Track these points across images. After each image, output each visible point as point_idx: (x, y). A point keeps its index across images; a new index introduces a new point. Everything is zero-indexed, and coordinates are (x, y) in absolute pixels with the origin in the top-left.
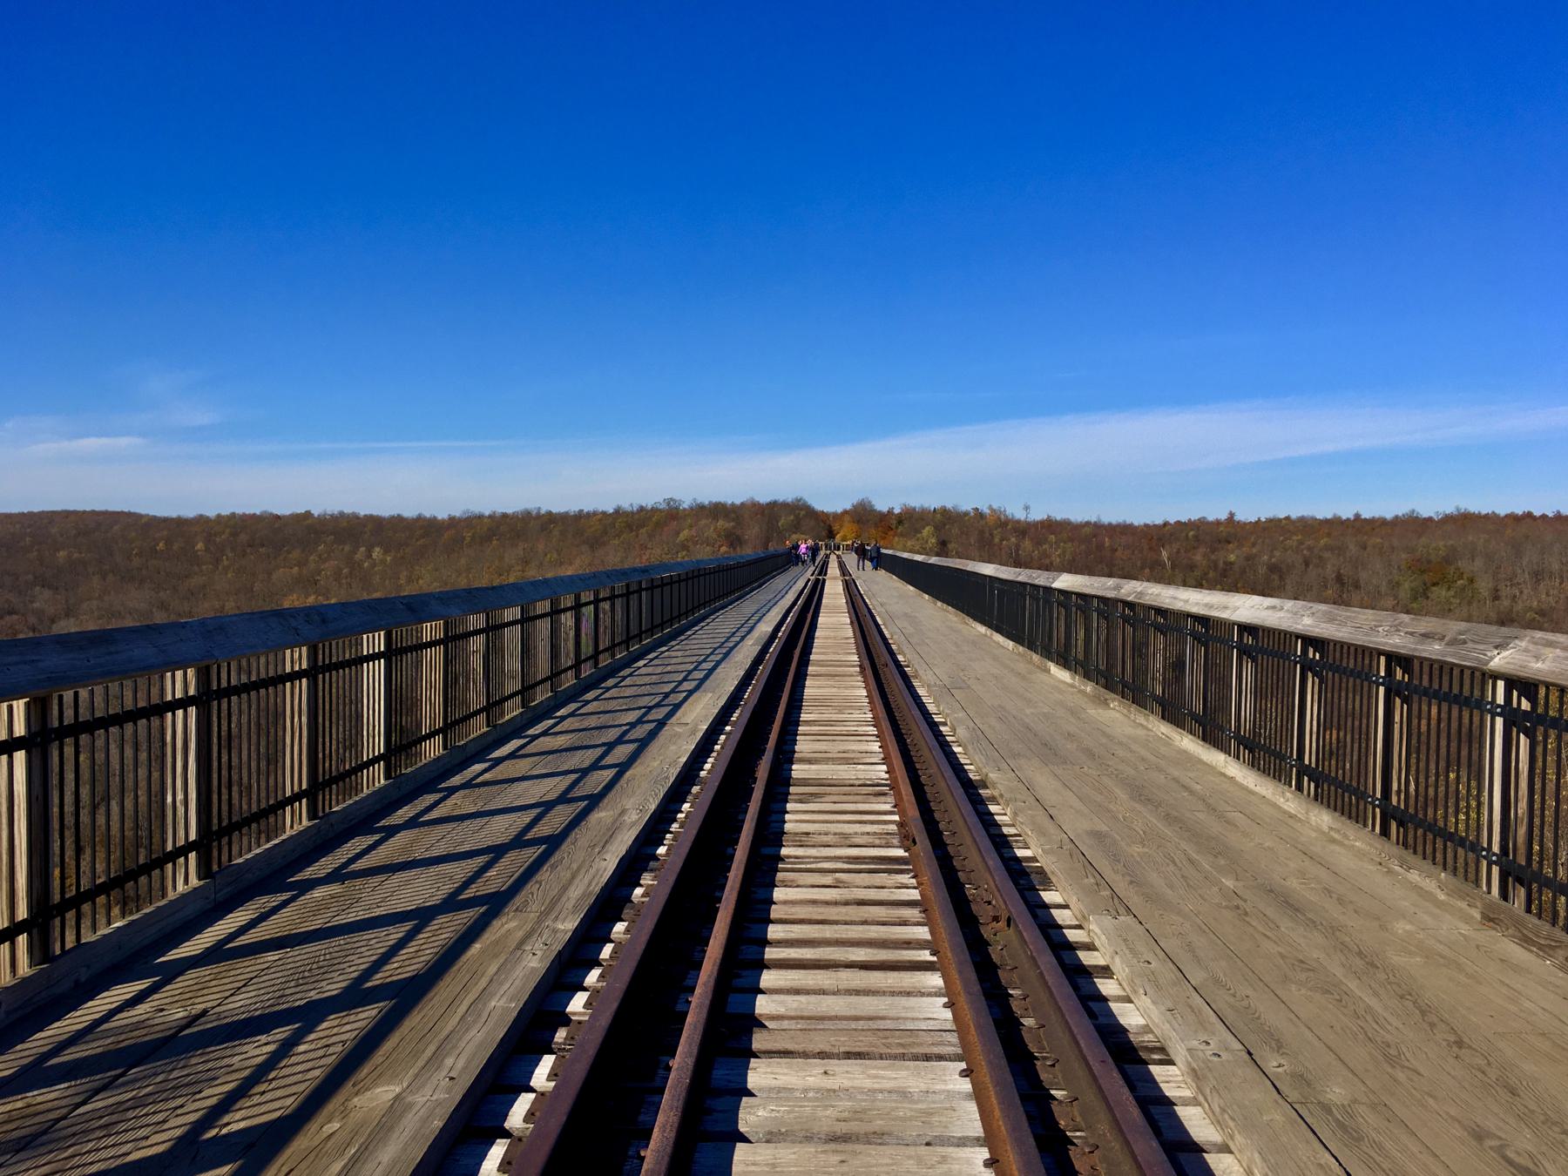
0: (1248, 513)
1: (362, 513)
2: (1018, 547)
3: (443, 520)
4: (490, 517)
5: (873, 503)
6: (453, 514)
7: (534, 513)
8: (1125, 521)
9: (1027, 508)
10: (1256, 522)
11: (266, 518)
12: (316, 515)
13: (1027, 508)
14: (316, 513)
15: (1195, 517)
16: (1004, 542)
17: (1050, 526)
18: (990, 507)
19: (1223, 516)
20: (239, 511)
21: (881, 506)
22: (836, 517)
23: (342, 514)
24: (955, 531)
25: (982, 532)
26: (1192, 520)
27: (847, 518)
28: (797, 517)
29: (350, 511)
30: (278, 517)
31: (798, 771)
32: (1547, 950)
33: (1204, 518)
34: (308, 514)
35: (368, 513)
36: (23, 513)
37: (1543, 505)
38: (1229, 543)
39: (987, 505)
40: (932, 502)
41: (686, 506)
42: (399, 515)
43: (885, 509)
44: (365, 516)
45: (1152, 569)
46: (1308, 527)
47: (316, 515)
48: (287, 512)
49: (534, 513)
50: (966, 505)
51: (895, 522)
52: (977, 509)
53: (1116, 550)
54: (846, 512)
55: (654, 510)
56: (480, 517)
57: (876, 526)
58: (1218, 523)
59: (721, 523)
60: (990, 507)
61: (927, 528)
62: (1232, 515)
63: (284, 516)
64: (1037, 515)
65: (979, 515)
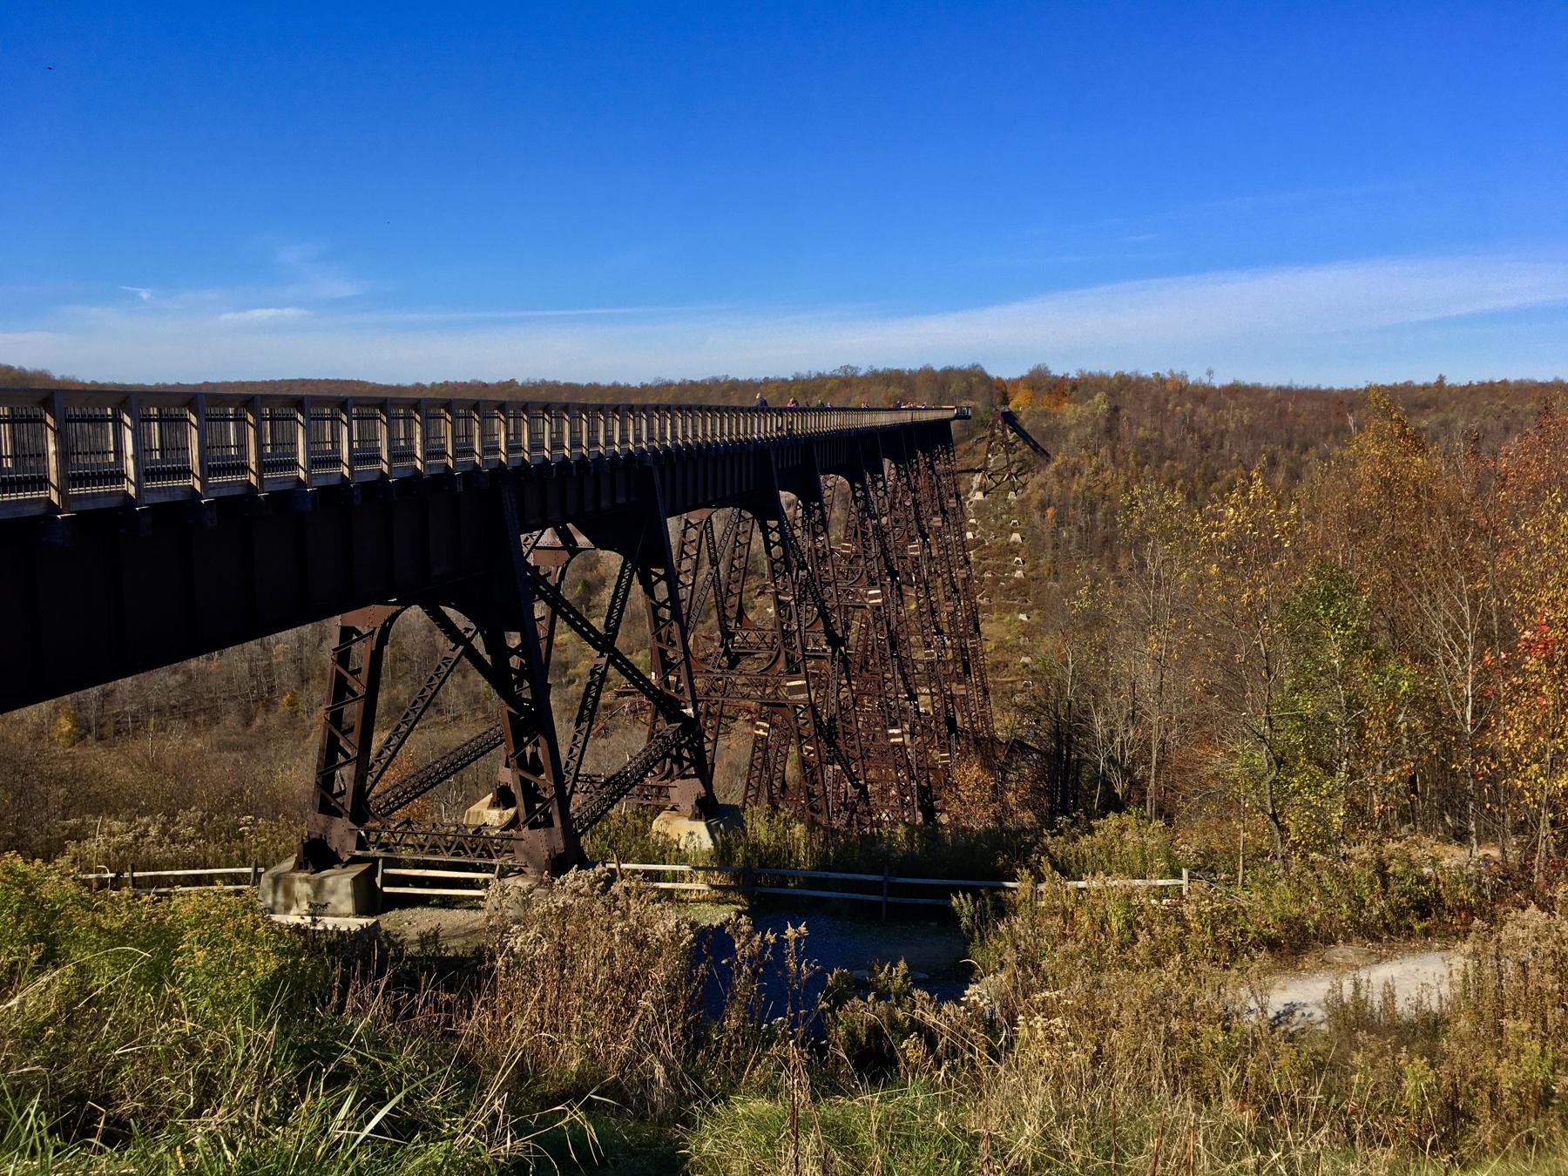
0: (1459, 376)
1: (563, 382)
2: (1193, 412)
3: (635, 388)
4: (680, 385)
5: (1050, 369)
6: (645, 382)
7: (722, 381)
8: (1319, 386)
9: (1210, 373)
10: (1468, 386)
11: (476, 386)
12: (520, 383)
13: (1210, 373)
14: (520, 381)
15: (1400, 381)
16: (1178, 408)
17: (1235, 390)
18: (1171, 372)
19: (1433, 380)
20: (452, 380)
21: (1057, 370)
22: (1015, 383)
23: (544, 383)
24: (1130, 396)
25: (1156, 398)
26: (1448, 382)
27: (1022, 384)
28: (970, 385)
29: (552, 380)
30: (485, 385)
31: (25, 425)
32: (685, 618)
33: (1411, 382)
34: (512, 383)
35: (568, 381)
36: (1492, 384)
37: (1543, 373)
38: (1428, 407)
39: (1168, 370)
40: (1109, 366)
41: (861, 373)
42: (554, 382)
43: (1061, 374)
44: (565, 384)
45: (1336, 434)
46: (1523, 390)
47: (520, 383)
48: (495, 381)
49: (722, 381)
50: (1147, 372)
51: (1069, 388)
52: (1158, 374)
53: (1299, 416)
54: (1022, 378)
55: (832, 377)
56: (669, 385)
57: (1050, 392)
58: (1425, 387)
59: (892, 389)
60: (1171, 372)
61: (1098, 395)
62: (1441, 379)
63: (493, 385)
64: (1221, 380)
65: (1162, 381)
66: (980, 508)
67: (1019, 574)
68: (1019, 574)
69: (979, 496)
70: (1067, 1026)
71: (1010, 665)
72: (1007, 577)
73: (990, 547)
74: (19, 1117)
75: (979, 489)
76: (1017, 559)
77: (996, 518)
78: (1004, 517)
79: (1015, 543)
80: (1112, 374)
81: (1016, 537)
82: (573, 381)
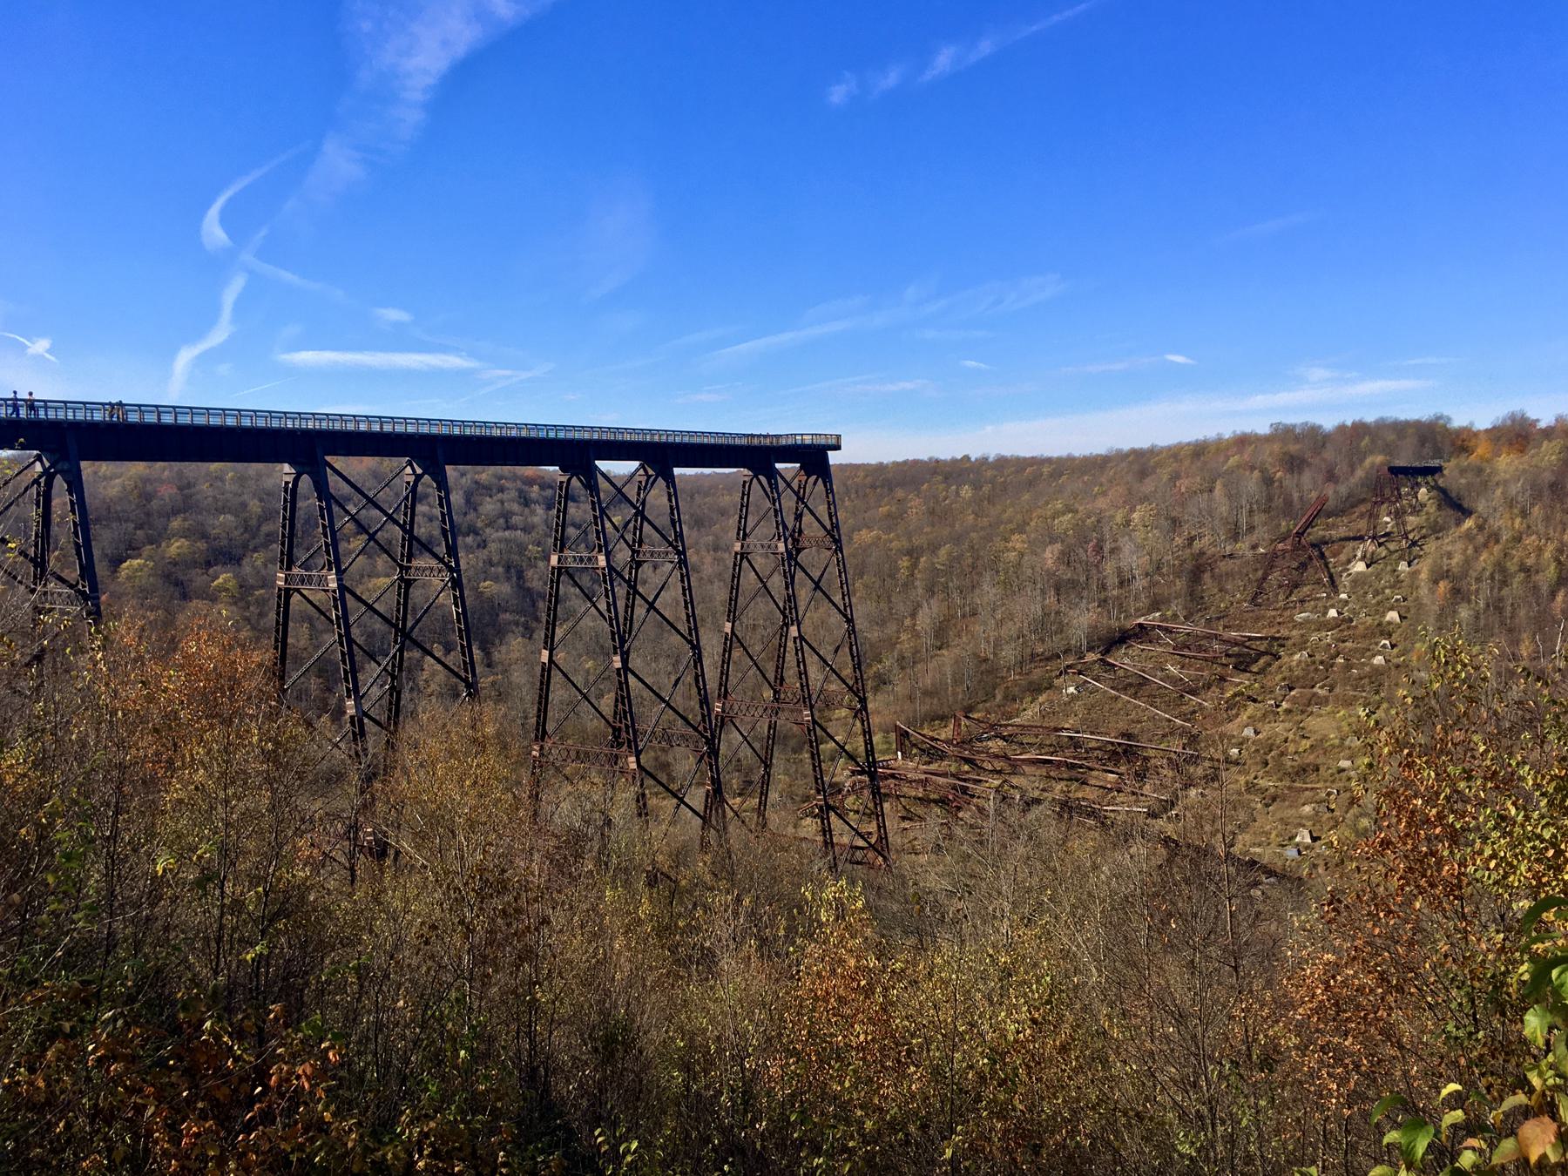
9: (31, 394)
12: (973, 459)
33: (1382, 419)
47: (973, 459)
66: (1358, 581)
67: (1378, 660)
68: (1378, 660)
69: (1360, 567)
70: (1517, 829)
71: (1322, 769)
72: (1363, 663)
73: (1356, 627)
74: (1161, 680)
75: (1363, 558)
76: (1383, 642)
77: (1376, 593)
78: (1387, 591)
79: (1389, 623)
80: (1349, 423)
81: (1393, 616)
82: (1138, 445)
